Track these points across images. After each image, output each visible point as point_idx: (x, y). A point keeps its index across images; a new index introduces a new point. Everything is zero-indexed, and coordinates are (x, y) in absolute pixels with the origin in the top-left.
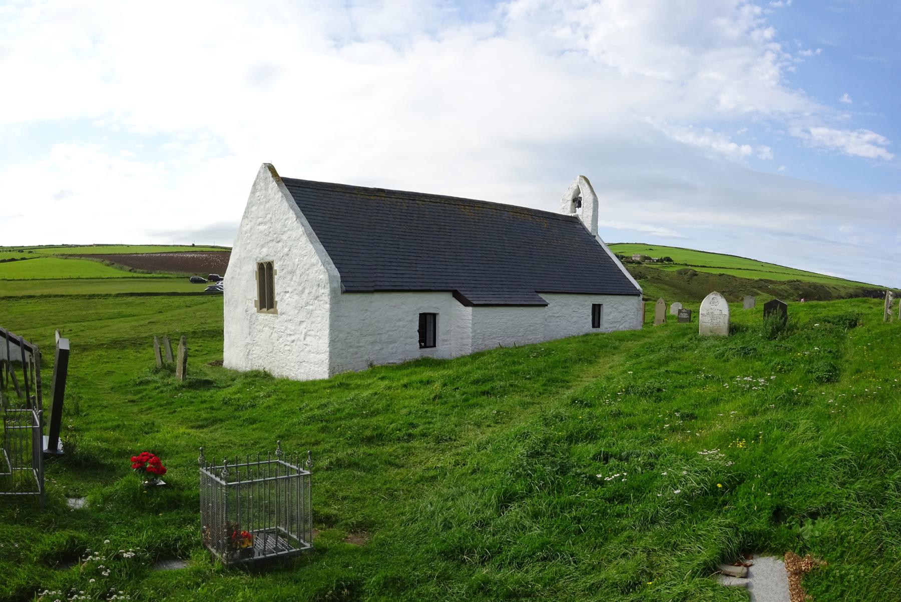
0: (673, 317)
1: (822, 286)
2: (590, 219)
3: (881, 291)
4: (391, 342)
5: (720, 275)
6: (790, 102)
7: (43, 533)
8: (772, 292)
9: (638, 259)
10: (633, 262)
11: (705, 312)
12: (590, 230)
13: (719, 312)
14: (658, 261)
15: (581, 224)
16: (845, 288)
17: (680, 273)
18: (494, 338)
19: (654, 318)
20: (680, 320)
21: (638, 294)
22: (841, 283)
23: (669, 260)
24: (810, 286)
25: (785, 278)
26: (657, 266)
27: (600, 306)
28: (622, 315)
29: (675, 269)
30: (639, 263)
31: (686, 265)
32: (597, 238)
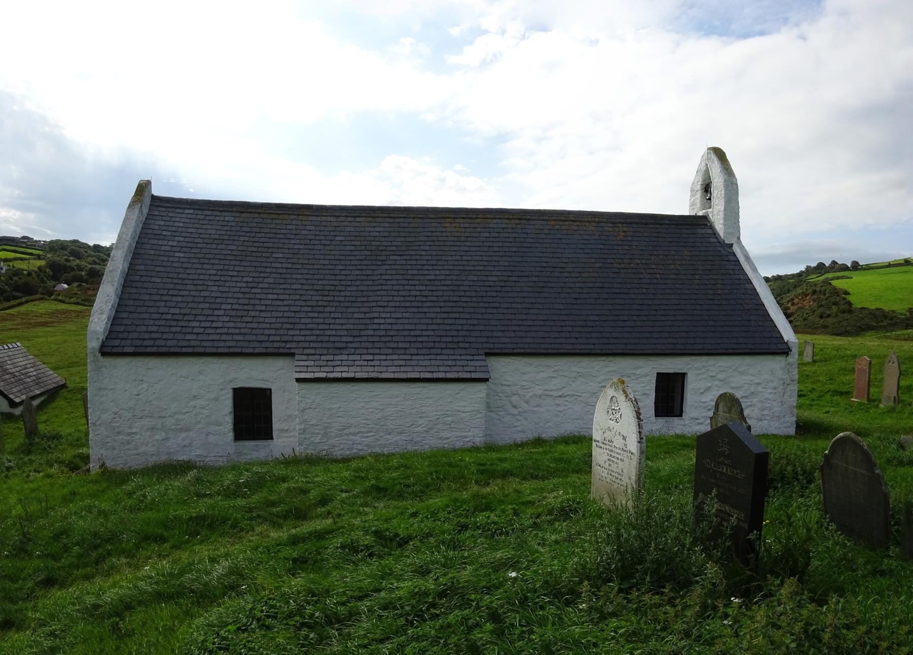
2: (722, 214)
4: (181, 430)
7: (710, 557)
12: (721, 234)
15: (711, 227)
18: (355, 434)
21: (783, 350)
27: (681, 377)
32: (736, 249)
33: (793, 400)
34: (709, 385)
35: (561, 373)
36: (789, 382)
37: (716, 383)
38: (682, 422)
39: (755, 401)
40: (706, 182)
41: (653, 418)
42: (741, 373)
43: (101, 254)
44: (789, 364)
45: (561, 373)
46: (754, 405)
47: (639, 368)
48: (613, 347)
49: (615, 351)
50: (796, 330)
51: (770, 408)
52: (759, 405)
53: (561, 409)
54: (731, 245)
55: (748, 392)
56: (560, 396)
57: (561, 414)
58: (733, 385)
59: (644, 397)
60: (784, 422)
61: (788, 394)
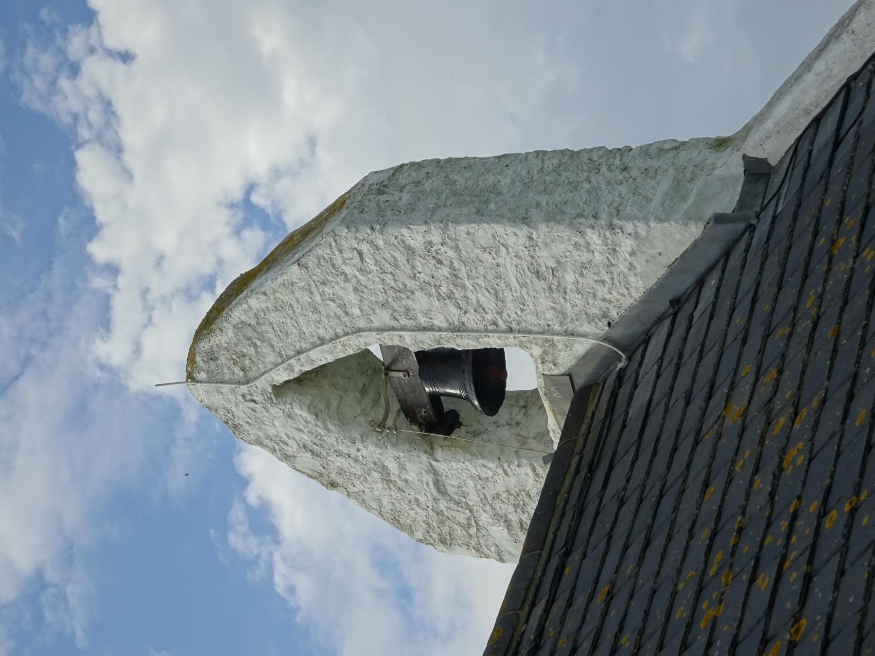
2: (555, 243)
15: (631, 344)
32: (773, 148)
54: (756, 171)
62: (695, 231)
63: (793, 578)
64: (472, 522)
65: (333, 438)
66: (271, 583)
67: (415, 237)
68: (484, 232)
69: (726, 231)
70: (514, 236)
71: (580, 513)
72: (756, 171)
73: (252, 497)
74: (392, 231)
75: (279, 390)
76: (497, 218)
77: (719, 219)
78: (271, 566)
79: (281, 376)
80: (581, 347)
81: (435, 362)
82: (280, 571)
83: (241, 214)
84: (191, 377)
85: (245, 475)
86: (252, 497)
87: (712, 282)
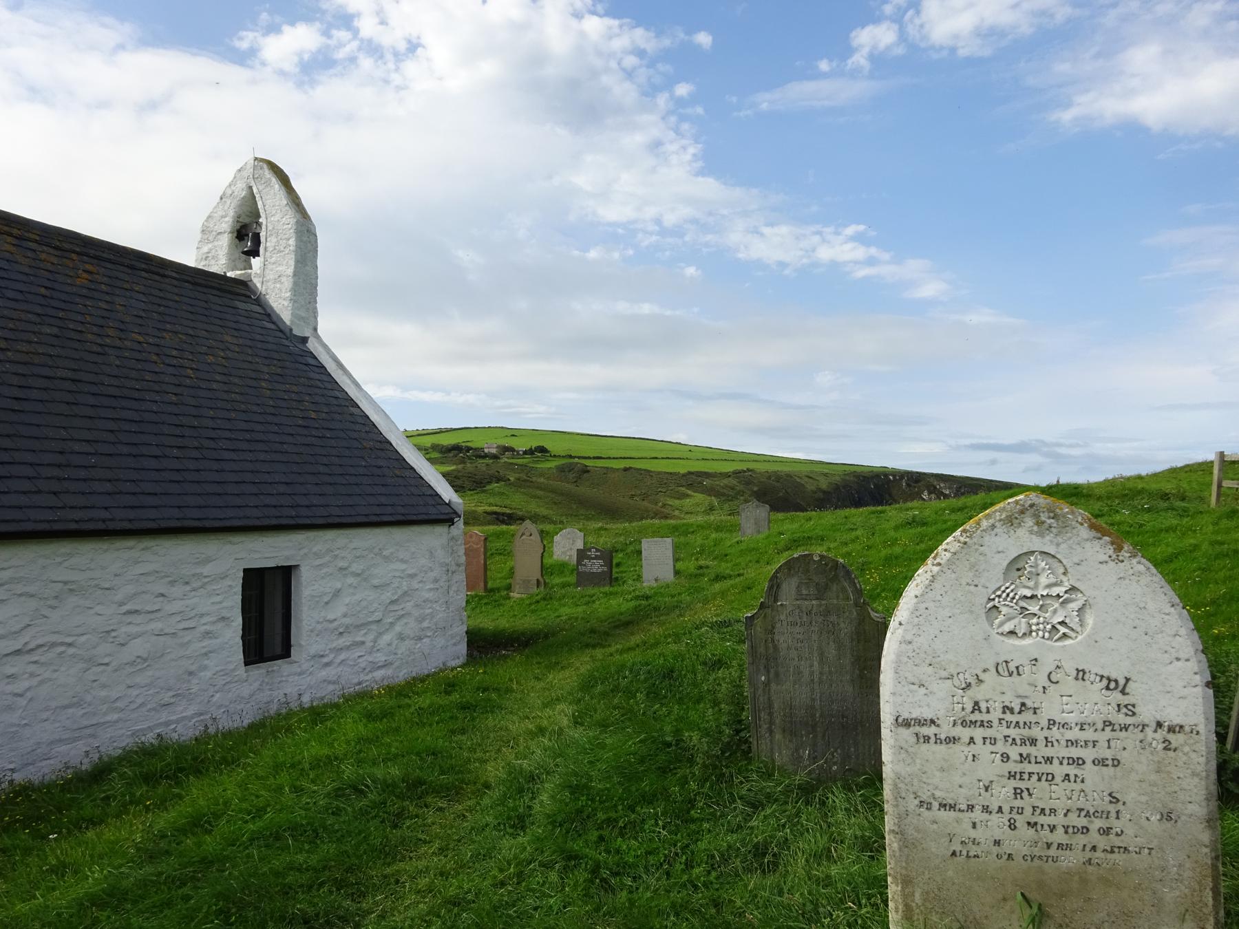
0: (561, 567)
1: (789, 475)
2: (288, 283)
3: (886, 475)
5: (626, 470)
6: (709, 188)
8: (710, 491)
9: (494, 451)
10: (486, 456)
11: (937, 703)
12: (286, 316)
13: (1096, 702)
14: (525, 453)
15: (259, 301)
16: (826, 475)
17: (561, 469)
19: (512, 572)
20: (585, 579)
21: (445, 517)
22: (817, 469)
23: (542, 450)
24: (769, 478)
25: (729, 468)
26: (525, 461)
27: (286, 574)
28: (387, 596)
29: (552, 464)
30: (495, 457)
31: (571, 457)
32: (312, 345)
33: (460, 596)
34: (339, 585)
35: (20, 589)
36: (454, 568)
37: (351, 580)
38: (295, 668)
39: (409, 606)
40: (247, 220)
41: (242, 670)
42: (387, 559)
43: (1212, 462)
44: (453, 538)
45: (20, 589)
46: (409, 614)
47: (208, 560)
48: (152, 514)
49: (164, 524)
50: (458, 489)
51: (432, 616)
52: (416, 613)
53: (19, 687)
54: (304, 340)
55: (400, 592)
56: (18, 652)
57: (22, 702)
58: (376, 582)
59: (220, 625)
60: (452, 637)
61: (454, 588)
62: (288, 323)
63: (175, 362)
64: (209, 242)
65: (235, 202)
66: (246, 30)
67: (292, 242)
68: (292, 263)
69: (287, 331)
70: (290, 271)
71: (206, 287)
72: (304, 340)
73: (286, 28)
74: (294, 235)
75: (251, 188)
76: (296, 267)
77: (291, 330)
78: (252, 30)
79: (255, 190)
80: (259, 285)
81: (257, 240)
82: (251, 35)
83: (415, 41)
84: (256, 159)
85: (298, 25)
86: (286, 28)
87: (273, 327)
